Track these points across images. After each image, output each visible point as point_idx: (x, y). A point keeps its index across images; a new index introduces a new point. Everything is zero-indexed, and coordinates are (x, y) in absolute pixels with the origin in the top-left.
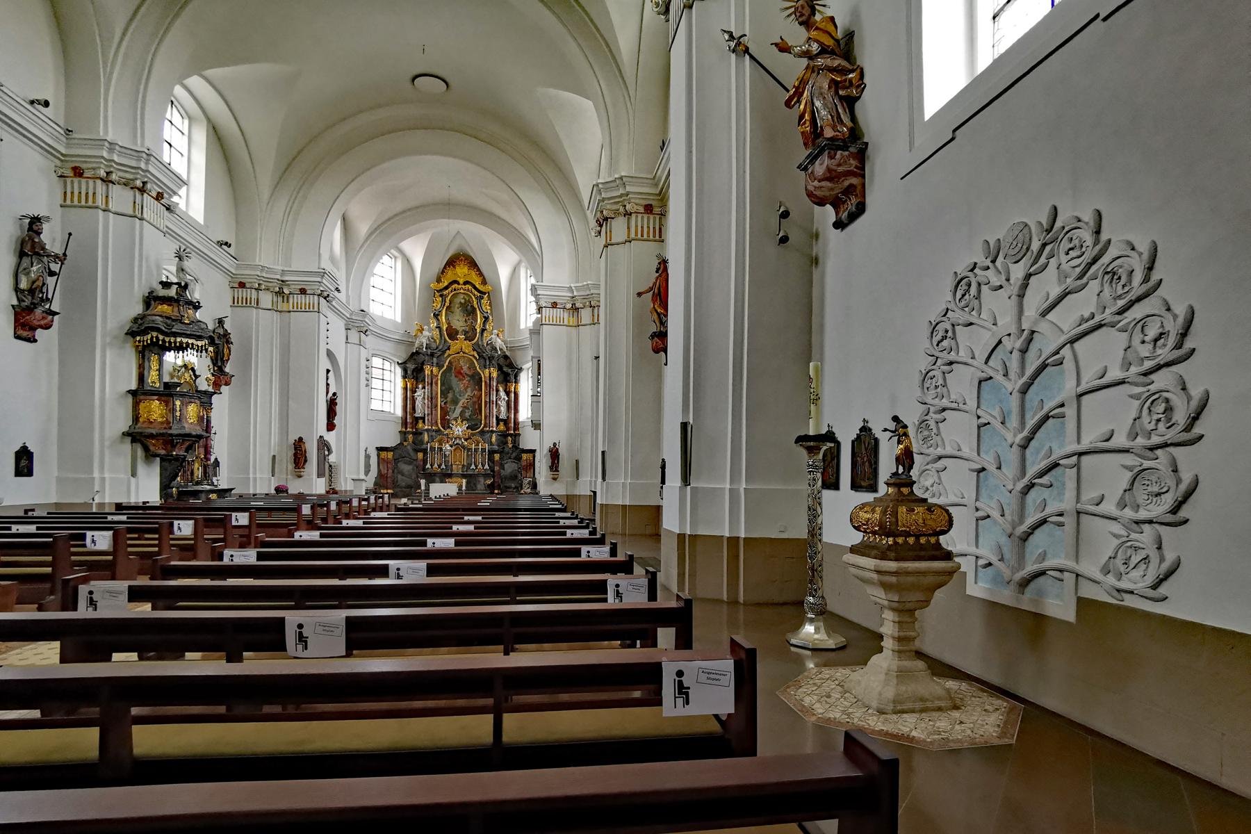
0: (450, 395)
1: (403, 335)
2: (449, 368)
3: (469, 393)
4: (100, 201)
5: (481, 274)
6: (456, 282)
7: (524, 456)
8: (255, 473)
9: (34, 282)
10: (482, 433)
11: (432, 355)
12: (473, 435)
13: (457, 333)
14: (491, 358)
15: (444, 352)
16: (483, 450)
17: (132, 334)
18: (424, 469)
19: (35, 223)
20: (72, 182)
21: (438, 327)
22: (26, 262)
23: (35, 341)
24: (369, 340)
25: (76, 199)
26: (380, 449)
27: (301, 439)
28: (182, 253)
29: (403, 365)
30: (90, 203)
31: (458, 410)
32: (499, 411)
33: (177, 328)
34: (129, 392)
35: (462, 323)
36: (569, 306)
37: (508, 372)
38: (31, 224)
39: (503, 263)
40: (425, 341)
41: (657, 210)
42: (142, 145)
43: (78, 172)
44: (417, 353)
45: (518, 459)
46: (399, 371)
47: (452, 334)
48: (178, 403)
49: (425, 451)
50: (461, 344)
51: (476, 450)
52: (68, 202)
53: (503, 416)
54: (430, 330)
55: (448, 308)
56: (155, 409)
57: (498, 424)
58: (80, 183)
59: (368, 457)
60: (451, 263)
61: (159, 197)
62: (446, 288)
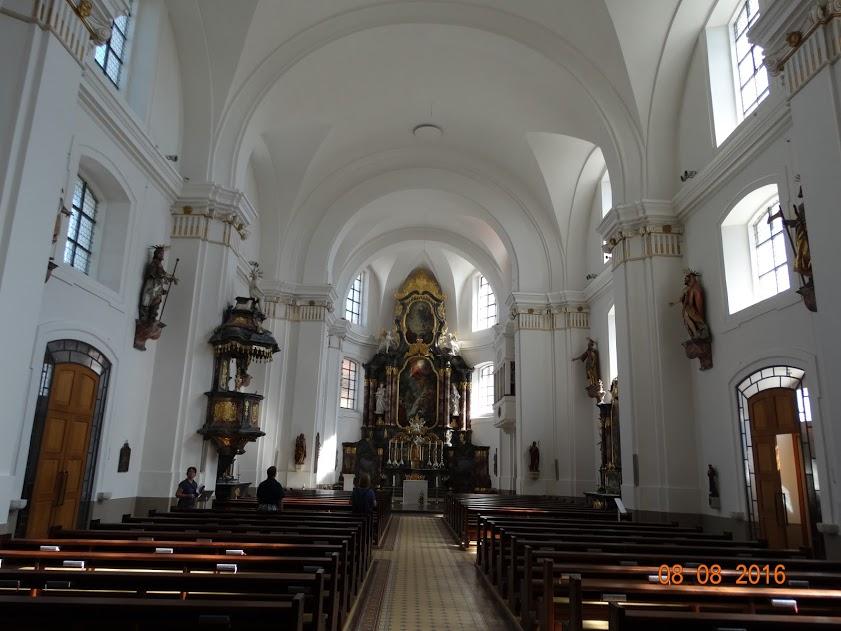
0: (408, 393)
1: (369, 339)
3: (425, 391)
4: (201, 233)
5: (438, 285)
12: (429, 431)
13: (415, 336)
19: (159, 251)
20: (182, 219)
24: (345, 344)
25: (189, 232)
27: (302, 436)
29: (367, 367)
30: (194, 235)
33: (254, 337)
34: (206, 394)
35: (419, 328)
39: (460, 272)
44: (380, 355)
45: (472, 455)
46: (363, 372)
47: (412, 337)
48: (247, 404)
52: (177, 234)
53: (456, 413)
54: (392, 335)
56: (228, 409)
57: (451, 421)
58: (187, 219)
59: (496, 472)
60: (414, 275)
61: (239, 228)
62: (407, 298)
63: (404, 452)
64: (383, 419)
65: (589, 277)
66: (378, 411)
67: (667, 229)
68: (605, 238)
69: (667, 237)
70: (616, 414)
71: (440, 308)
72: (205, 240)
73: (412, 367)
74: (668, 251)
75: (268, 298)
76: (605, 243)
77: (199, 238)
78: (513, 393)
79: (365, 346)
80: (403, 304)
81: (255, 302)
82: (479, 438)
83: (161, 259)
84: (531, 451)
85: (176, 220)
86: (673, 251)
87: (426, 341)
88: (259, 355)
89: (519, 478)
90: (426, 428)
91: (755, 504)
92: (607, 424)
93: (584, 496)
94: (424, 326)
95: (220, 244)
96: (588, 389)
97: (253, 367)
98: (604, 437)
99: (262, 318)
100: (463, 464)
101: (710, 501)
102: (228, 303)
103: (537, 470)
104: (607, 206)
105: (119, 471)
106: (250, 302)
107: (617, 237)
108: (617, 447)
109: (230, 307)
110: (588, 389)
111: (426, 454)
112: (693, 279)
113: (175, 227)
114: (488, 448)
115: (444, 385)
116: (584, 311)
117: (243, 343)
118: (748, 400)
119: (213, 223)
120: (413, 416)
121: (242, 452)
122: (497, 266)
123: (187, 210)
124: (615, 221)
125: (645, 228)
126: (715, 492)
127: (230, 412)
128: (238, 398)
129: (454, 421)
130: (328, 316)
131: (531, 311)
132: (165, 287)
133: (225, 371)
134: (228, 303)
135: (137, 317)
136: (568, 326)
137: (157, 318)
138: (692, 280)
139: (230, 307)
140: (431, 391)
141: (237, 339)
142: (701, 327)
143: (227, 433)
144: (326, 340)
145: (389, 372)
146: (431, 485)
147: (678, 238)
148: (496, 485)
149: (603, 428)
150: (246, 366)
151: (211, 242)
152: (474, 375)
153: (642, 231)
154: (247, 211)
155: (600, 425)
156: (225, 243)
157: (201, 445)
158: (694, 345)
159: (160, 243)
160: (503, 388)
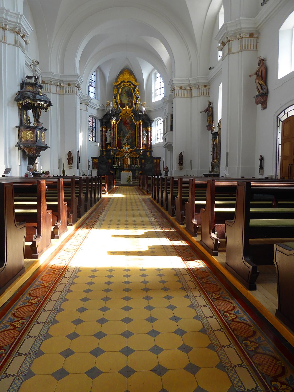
0: (122, 133)
1: (101, 107)
5: (135, 78)
6: (124, 81)
10: (136, 150)
14: (140, 116)
16: (138, 158)
17: (17, 100)
26: (93, 158)
27: (70, 152)
29: (101, 121)
31: (125, 140)
34: (16, 127)
36: (188, 88)
39: (146, 71)
41: (255, 36)
45: (153, 162)
46: (99, 123)
48: (38, 132)
49: (112, 159)
50: (127, 108)
51: (134, 158)
54: (113, 104)
55: (121, 94)
57: (142, 146)
60: (122, 72)
62: (119, 84)
63: (121, 161)
64: (110, 146)
65: (210, 69)
67: (251, 35)
68: (219, 42)
70: (220, 137)
71: (137, 90)
76: (219, 45)
78: (172, 130)
80: (118, 88)
81: (37, 79)
82: (156, 154)
84: (179, 156)
90: (131, 149)
91: (279, 170)
95: (14, 45)
96: (207, 126)
98: (213, 148)
100: (149, 166)
101: (259, 171)
103: (182, 165)
104: (221, 22)
107: (225, 41)
108: (219, 152)
109: (23, 81)
110: (207, 126)
111: (131, 161)
112: (262, 62)
114: (160, 158)
115: (139, 129)
116: (207, 87)
117: (32, 100)
118: (282, 122)
119: (7, 33)
120: (125, 144)
121: (39, 156)
122: (166, 67)
124: (225, 31)
125: (240, 34)
126: (262, 167)
127: (30, 136)
129: (144, 146)
131: (181, 88)
136: (199, 96)
138: (262, 62)
140: (133, 132)
141: (28, 98)
142: (264, 87)
149: (213, 144)
150: (39, 117)
151: (8, 44)
152: (154, 124)
153: (238, 36)
156: (16, 44)
158: (260, 97)
160: (167, 128)
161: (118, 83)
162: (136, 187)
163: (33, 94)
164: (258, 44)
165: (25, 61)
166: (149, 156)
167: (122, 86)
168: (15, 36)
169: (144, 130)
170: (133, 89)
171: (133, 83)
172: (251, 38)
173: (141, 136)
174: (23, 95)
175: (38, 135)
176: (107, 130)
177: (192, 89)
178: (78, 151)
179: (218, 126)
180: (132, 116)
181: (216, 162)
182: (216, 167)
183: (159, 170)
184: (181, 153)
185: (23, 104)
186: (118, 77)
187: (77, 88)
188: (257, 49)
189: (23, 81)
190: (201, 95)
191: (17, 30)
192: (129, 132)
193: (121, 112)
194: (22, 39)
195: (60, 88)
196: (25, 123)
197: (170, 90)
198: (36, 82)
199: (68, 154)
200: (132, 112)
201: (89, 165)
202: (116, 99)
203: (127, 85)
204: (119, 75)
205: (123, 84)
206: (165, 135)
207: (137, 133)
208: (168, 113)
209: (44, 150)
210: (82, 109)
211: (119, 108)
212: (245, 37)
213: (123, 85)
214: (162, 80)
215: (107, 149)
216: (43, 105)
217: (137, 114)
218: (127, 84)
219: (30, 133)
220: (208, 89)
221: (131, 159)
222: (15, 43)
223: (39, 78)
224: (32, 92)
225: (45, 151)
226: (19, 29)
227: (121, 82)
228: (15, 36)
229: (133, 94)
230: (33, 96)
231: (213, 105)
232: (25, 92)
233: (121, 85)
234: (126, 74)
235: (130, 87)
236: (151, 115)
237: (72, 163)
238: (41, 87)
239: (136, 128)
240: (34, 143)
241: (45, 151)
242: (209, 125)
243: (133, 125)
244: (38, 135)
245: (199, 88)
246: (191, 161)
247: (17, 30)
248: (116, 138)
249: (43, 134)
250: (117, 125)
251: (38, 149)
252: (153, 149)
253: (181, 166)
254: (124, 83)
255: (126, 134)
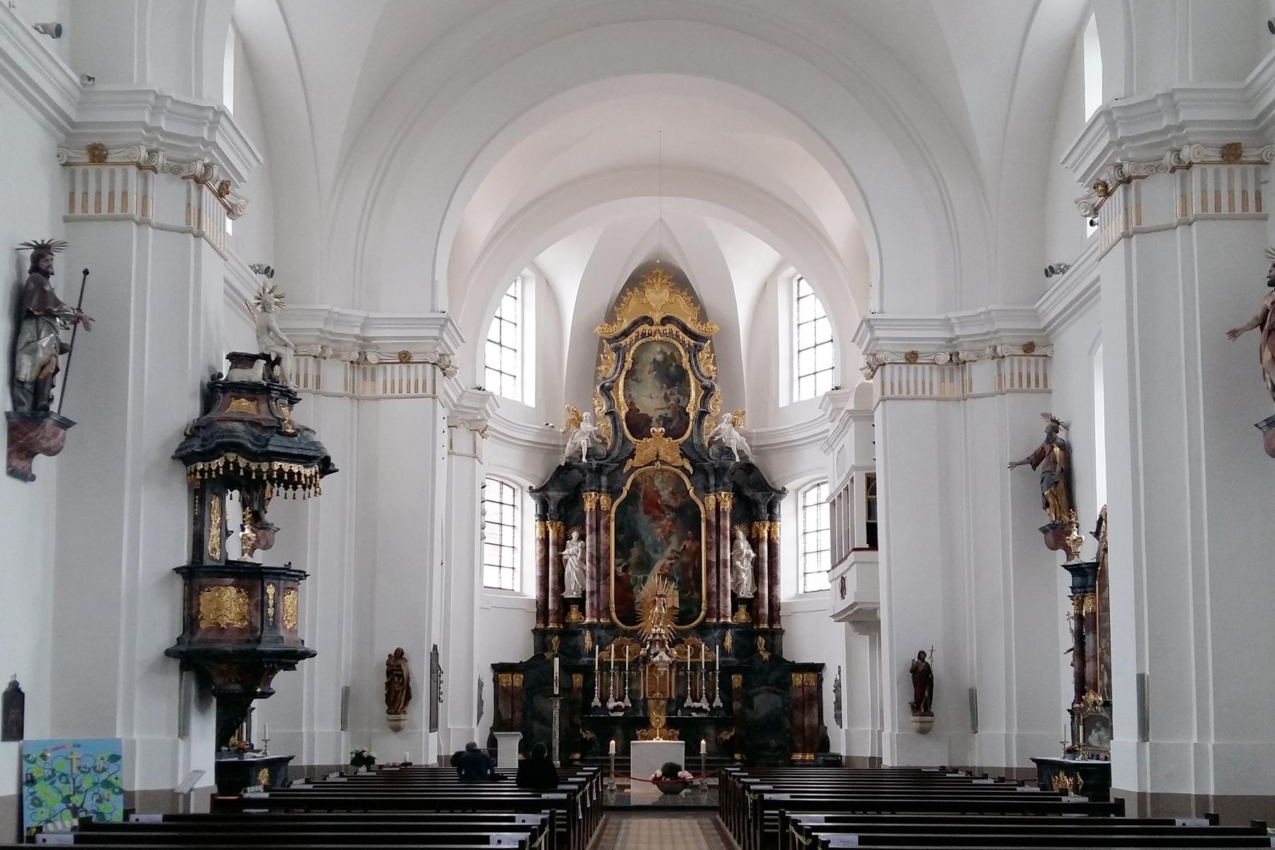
0: (635, 552)
2: (633, 495)
3: (674, 544)
4: (134, 209)
5: (695, 301)
6: (647, 320)
7: (797, 679)
8: (311, 724)
9: (43, 367)
11: (599, 470)
13: (648, 420)
14: (719, 472)
15: (622, 463)
16: (710, 666)
17: (185, 457)
18: (586, 707)
20: (86, 173)
21: (611, 413)
22: (29, 329)
23: (33, 478)
24: (485, 445)
26: (499, 669)
27: (399, 654)
28: (271, 298)
30: (117, 211)
32: (737, 583)
33: (276, 444)
34: (178, 570)
37: (755, 496)
38: (36, 259)
40: (584, 444)
41: (1250, 154)
42: (199, 95)
43: (98, 154)
44: (568, 467)
45: (783, 685)
46: (531, 505)
47: (639, 425)
48: (270, 590)
49: (588, 671)
50: (658, 447)
52: (78, 212)
53: (746, 591)
54: (595, 420)
55: (630, 374)
56: (227, 604)
59: (838, 718)
60: (637, 281)
61: (221, 193)
62: (625, 334)
66: (571, 592)
67: (1231, 153)
69: (1230, 173)
72: (143, 222)
73: (656, 483)
74: (1021, 385)
75: (301, 350)
77: (131, 219)
78: (873, 543)
79: (532, 447)
80: (616, 349)
81: (272, 363)
83: (47, 274)
84: (914, 670)
85: (73, 174)
86: (1029, 382)
87: (673, 433)
88: (291, 481)
89: (887, 731)
92: (1088, 607)
93: (1034, 765)
94: (666, 398)
95: (182, 231)
96: (1044, 530)
97: (278, 506)
99: (292, 399)
100: (764, 703)
102: (211, 368)
103: (927, 712)
105: (4, 740)
106: (261, 363)
107: (1108, 176)
110: (1044, 530)
113: (72, 194)
121: (266, 694)
123: (98, 154)
125: (1178, 152)
128: (249, 577)
129: (742, 609)
130: (443, 384)
131: (912, 358)
132: (65, 337)
133: (216, 519)
134: (211, 368)
135: (9, 407)
137: (54, 408)
139: (216, 377)
140: (688, 544)
141: (238, 448)
143: (228, 668)
144: (443, 439)
145: (589, 506)
146: (692, 750)
147: (1257, 172)
148: (839, 746)
149: (1079, 618)
150: (263, 506)
152: (785, 507)
154: (238, 153)
155: (1072, 610)
157: (176, 679)
159: (42, 236)
161: (618, 329)
162: (707, 821)
163: (256, 431)
164: (1263, 188)
165: (226, 281)
166: (766, 656)
167: (637, 339)
168: (189, 192)
169: (741, 535)
170: (688, 351)
171: (690, 325)
172: (1229, 162)
173: (725, 561)
174: (212, 436)
175: (271, 603)
176: (568, 537)
177: (964, 362)
178: (435, 647)
179: (1097, 534)
180: (683, 468)
181: (1091, 714)
182: (1098, 725)
183: (816, 721)
184: (922, 655)
185: (210, 475)
186: (619, 301)
187: (438, 370)
188: (1263, 212)
189: (213, 378)
190: (1008, 386)
191: (199, 168)
192: (669, 543)
193: (632, 456)
194: (216, 201)
195: (364, 369)
196: (214, 549)
197: (863, 363)
198: (270, 377)
199: (388, 664)
200: (683, 455)
201: (481, 703)
202: (610, 398)
203: (658, 332)
204: (623, 292)
205: (640, 329)
206: (840, 562)
207: (708, 549)
208: (854, 468)
209: (290, 667)
210: (455, 449)
211: (624, 436)
212: (1203, 163)
213: (643, 336)
214: (821, 311)
215: (564, 623)
216: (299, 474)
217: (705, 461)
218: (661, 328)
219: (233, 596)
220: (1041, 359)
221: (681, 673)
222: (188, 222)
223: (283, 362)
224: (254, 424)
225: (294, 669)
226: (207, 167)
227: (635, 324)
228: (189, 192)
229: (690, 373)
230: (257, 439)
231: (1067, 436)
232: (223, 425)
233: (633, 335)
234: (657, 287)
235: (676, 343)
236: (775, 473)
237: (406, 704)
238: (292, 399)
239: (703, 525)
240: (248, 641)
241: (294, 669)
242: (1053, 526)
243: (688, 517)
244: (271, 603)
245: (997, 357)
246: (973, 695)
247: (199, 168)
248: (609, 575)
249: (289, 599)
250: (613, 515)
251: (268, 663)
252: (784, 624)
253: (922, 715)
254: (646, 327)
255: (656, 551)
